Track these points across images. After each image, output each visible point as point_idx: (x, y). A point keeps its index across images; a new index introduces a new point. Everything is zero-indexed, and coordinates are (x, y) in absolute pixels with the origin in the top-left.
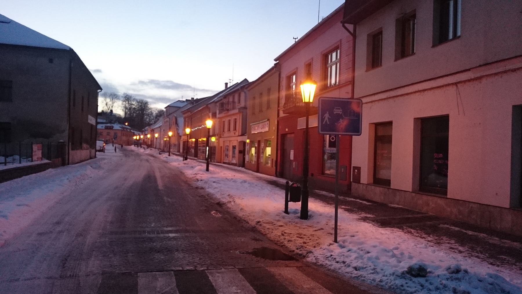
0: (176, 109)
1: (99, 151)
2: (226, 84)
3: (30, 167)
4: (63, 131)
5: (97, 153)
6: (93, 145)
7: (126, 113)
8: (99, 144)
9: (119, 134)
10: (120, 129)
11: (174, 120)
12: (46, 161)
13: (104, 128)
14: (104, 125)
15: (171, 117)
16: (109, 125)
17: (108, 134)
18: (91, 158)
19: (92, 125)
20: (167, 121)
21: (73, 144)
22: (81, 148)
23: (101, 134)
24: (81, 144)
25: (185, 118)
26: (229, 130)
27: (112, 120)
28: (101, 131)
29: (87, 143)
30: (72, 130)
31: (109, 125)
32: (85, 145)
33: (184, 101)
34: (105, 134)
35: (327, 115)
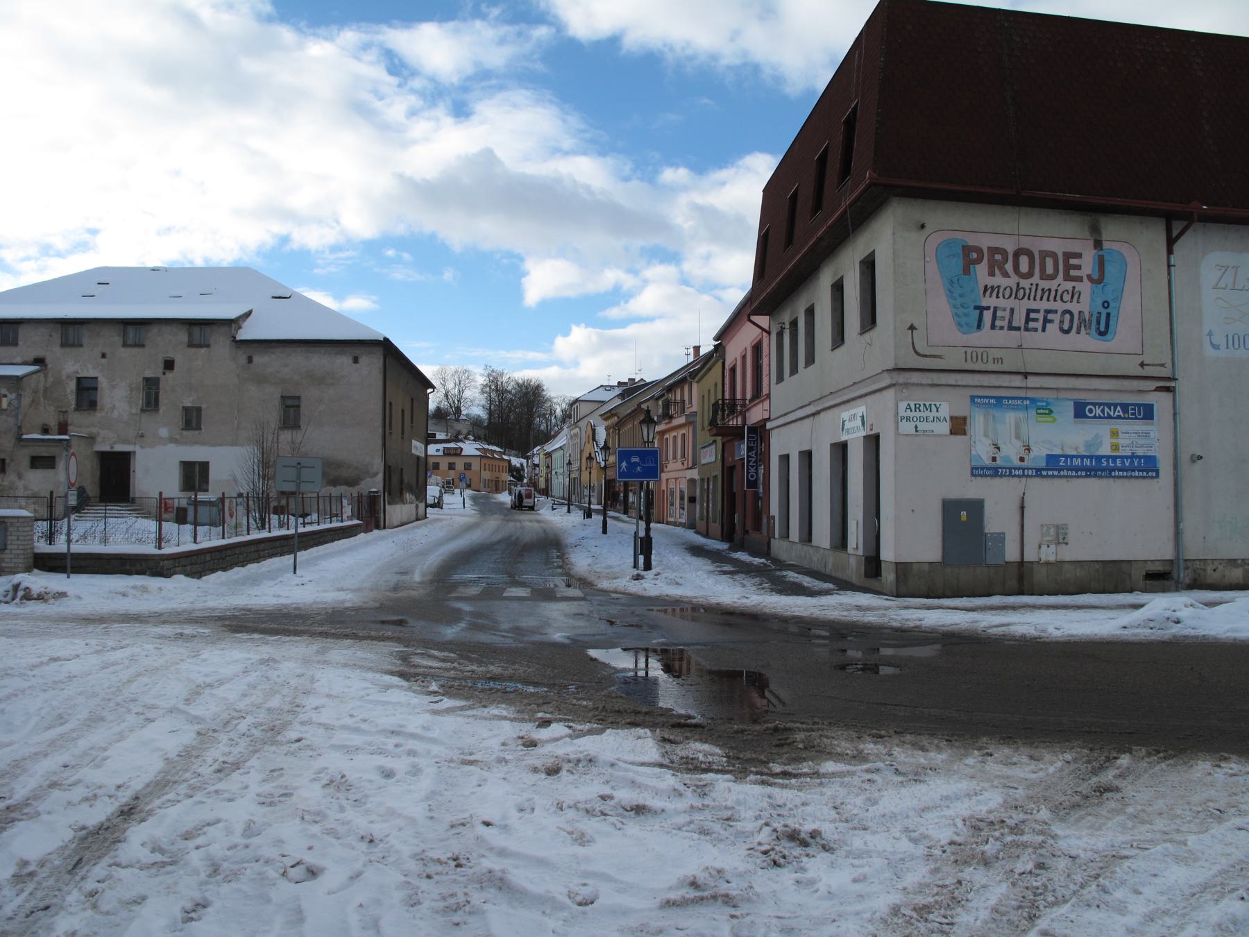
0: (595, 406)
1: (432, 506)
2: (697, 349)
3: (341, 529)
4: (376, 474)
5: (429, 510)
6: (420, 493)
7: (490, 413)
8: (433, 491)
9: (476, 465)
10: (478, 453)
11: (590, 432)
12: (356, 522)
13: (441, 453)
14: (441, 446)
15: (580, 424)
16: (452, 445)
17: (451, 466)
18: (417, 519)
19: (418, 458)
20: (576, 435)
21: (390, 494)
22: (403, 501)
23: (436, 466)
24: (401, 493)
25: (607, 429)
26: (675, 457)
27: (459, 433)
28: (436, 460)
29: (411, 491)
30: (388, 470)
31: (452, 445)
32: (408, 496)
33: (612, 387)
34: (444, 466)
35: (624, 464)
